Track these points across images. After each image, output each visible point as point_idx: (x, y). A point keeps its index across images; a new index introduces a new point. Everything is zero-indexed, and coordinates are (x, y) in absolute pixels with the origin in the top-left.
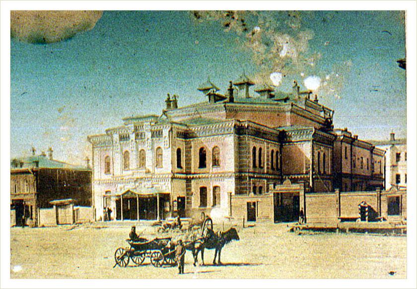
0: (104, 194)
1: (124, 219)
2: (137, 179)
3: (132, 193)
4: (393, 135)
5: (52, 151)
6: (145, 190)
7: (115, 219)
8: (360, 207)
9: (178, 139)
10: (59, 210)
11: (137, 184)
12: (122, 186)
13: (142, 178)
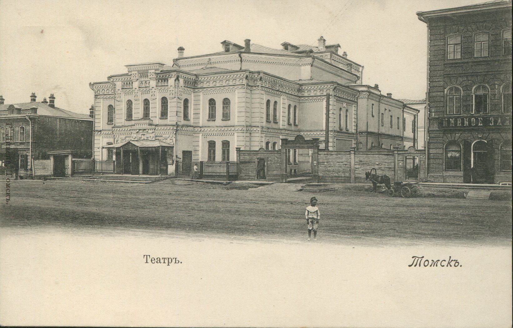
11: (140, 136)
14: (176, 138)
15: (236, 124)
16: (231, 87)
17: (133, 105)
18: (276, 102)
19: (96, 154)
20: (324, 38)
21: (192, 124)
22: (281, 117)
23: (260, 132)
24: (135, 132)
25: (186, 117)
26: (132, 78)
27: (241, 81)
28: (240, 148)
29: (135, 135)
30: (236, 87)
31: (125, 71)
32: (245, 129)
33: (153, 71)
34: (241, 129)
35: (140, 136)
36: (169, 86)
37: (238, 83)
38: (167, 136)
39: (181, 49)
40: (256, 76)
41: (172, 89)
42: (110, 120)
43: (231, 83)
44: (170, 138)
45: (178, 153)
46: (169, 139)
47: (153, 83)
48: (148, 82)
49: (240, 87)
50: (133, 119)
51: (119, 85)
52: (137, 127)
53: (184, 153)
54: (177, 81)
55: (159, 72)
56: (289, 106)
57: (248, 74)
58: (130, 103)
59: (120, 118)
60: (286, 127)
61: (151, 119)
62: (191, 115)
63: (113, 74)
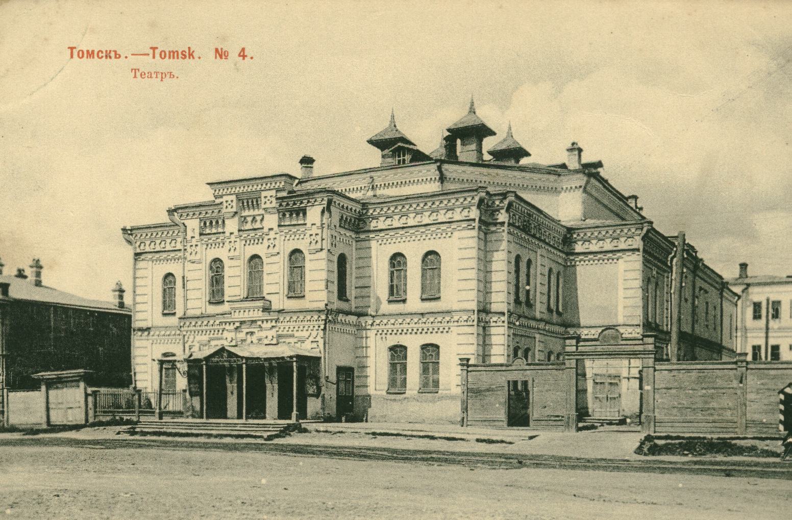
0: (160, 358)
1: (247, 418)
2: (242, 323)
3: (231, 354)
4: (744, 266)
5: (41, 267)
6: (258, 346)
7: (674, 360)
8: (782, 397)
9: (343, 231)
10: (52, 393)
11: (242, 335)
12: (205, 338)
13: (255, 321)
14: (324, 338)
15: (455, 307)
16: (443, 227)
17: (226, 269)
18: (529, 262)
19: (138, 377)
20: (580, 145)
21: (353, 310)
22: (538, 294)
23: (506, 324)
24: (232, 327)
25: (342, 294)
26: (224, 210)
27: (465, 213)
28: (468, 360)
29: (232, 335)
30: (454, 226)
31: (206, 195)
32: (475, 317)
33: (273, 193)
34: (465, 318)
35: (242, 335)
36: (309, 225)
37: (457, 216)
38: (306, 334)
39: (307, 161)
40: (497, 203)
41: (315, 230)
42: (168, 308)
43: (442, 218)
44: (311, 339)
45: (328, 371)
46: (308, 342)
47: (272, 221)
48: (259, 218)
49: (464, 225)
50: (226, 298)
51: (193, 225)
52: (238, 316)
53: (340, 370)
54: (326, 214)
55: (284, 194)
56: (550, 270)
57: (483, 194)
58: (217, 266)
59: (195, 297)
60: (546, 316)
61: (267, 297)
62: (351, 292)
63: (181, 203)
